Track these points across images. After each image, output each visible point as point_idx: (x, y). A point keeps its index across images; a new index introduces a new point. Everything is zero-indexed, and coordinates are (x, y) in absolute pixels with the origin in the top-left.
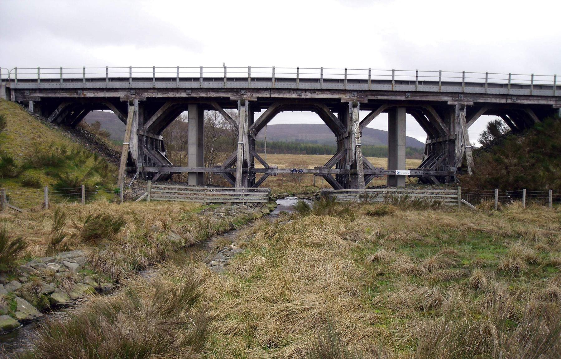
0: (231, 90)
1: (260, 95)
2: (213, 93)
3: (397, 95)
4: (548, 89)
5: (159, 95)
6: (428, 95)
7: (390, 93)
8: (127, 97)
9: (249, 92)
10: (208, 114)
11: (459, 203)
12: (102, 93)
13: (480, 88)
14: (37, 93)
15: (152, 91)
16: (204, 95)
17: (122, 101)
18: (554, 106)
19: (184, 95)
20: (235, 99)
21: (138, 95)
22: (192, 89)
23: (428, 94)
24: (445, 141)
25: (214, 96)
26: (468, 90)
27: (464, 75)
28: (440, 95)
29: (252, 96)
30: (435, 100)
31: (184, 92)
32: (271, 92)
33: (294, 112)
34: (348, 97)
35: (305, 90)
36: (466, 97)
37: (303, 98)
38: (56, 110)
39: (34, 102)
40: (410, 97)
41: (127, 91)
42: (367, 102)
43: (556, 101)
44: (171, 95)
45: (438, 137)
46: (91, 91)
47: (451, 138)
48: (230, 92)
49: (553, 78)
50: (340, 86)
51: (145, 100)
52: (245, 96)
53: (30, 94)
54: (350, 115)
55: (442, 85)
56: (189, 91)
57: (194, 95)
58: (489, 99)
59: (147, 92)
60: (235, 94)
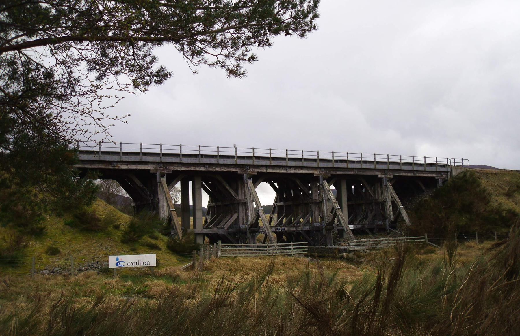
1: (259, 171)
2: (183, 167)
3: (348, 171)
4: (283, 161)
5: (183, 169)
7: (344, 169)
8: (157, 170)
9: (252, 167)
12: (134, 165)
13: (409, 166)
18: (436, 177)
20: (242, 173)
21: (165, 168)
22: (210, 165)
25: (226, 170)
26: (391, 167)
27: (287, 153)
29: (254, 171)
31: (203, 167)
32: (267, 168)
34: (319, 172)
35: (291, 167)
41: (156, 164)
42: (330, 176)
43: (437, 174)
44: (192, 169)
46: (125, 164)
48: (238, 167)
50: (314, 164)
52: (249, 171)
55: (288, 160)
57: (210, 169)
58: (401, 173)
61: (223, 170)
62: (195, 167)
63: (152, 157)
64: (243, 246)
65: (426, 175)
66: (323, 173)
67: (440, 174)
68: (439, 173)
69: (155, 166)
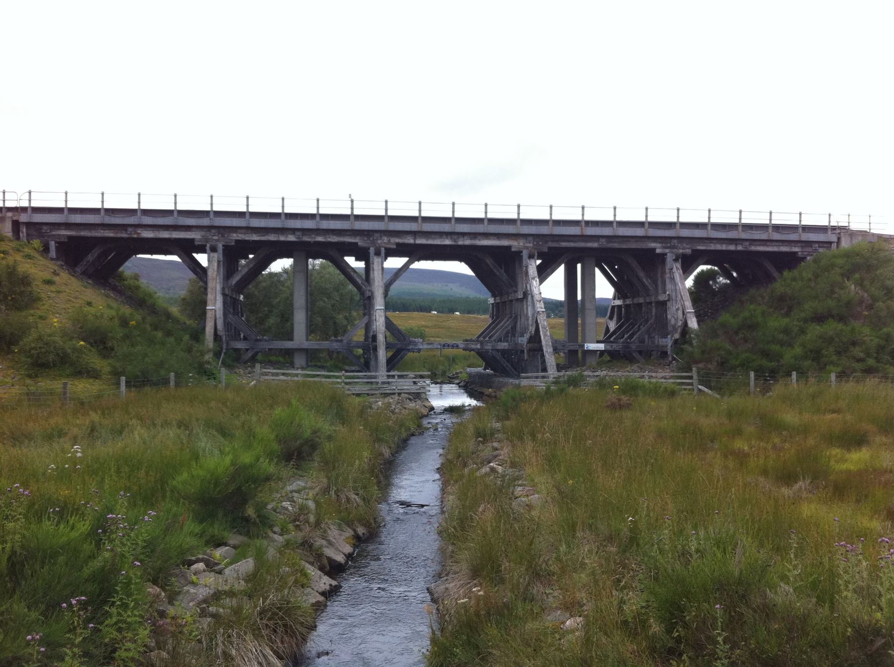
1: (398, 240)
5: (255, 237)
6: (629, 241)
9: (385, 235)
11: (696, 391)
12: (166, 232)
14: (61, 229)
15: (243, 231)
16: (320, 239)
17: (198, 245)
18: (800, 253)
22: (305, 231)
23: (629, 239)
25: (336, 240)
26: (685, 233)
28: (646, 240)
30: (639, 247)
31: (292, 234)
34: (521, 244)
35: (463, 234)
39: (56, 242)
40: (603, 243)
41: (205, 230)
42: (546, 250)
43: (802, 247)
44: (272, 237)
45: (636, 294)
50: (511, 229)
51: (233, 244)
52: (379, 242)
53: (50, 232)
54: (524, 268)
55: (680, 228)
56: (298, 233)
57: (306, 239)
58: (712, 245)
59: (236, 232)
60: (366, 239)
61: (329, 240)
62: (277, 235)
63: (339, 222)
64: (396, 377)
65: (775, 249)
66: (531, 245)
67: (811, 247)
68: (809, 243)
69: (203, 233)
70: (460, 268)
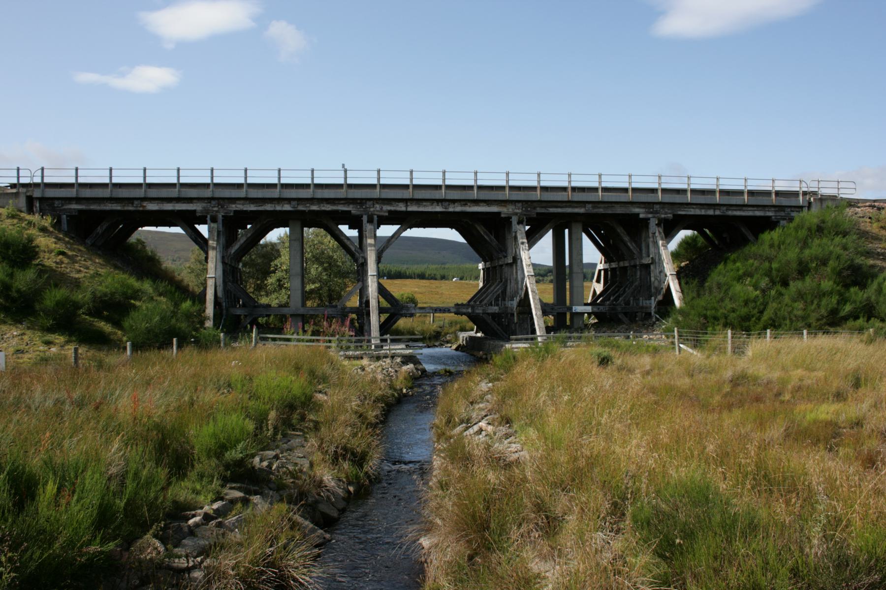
0: (353, 201)
2: (328, 206)
9: (378, 203)
10: (310, 232)
15: (242, 202)
16: (315, 208)
19: (287, 207)
24: (635, 266)
32: (407, 203)
33: (427, 229)
34: (511, 210)
35: (454, 201)
36: (663, 208)
37: (451, 212)
38: (99, 228)
40: (589, 209)
43: (776, 211)
44: (269, 207)
47: (646, 261)
48: (351, 203)
49: (108, 171)
51: (232, 214)
52: (372, 209)
53: (63, 205)
56: (294, 203)
57: (301, 208)
59: (235, 203)
69: (204, 205)
70: (451, 235)
